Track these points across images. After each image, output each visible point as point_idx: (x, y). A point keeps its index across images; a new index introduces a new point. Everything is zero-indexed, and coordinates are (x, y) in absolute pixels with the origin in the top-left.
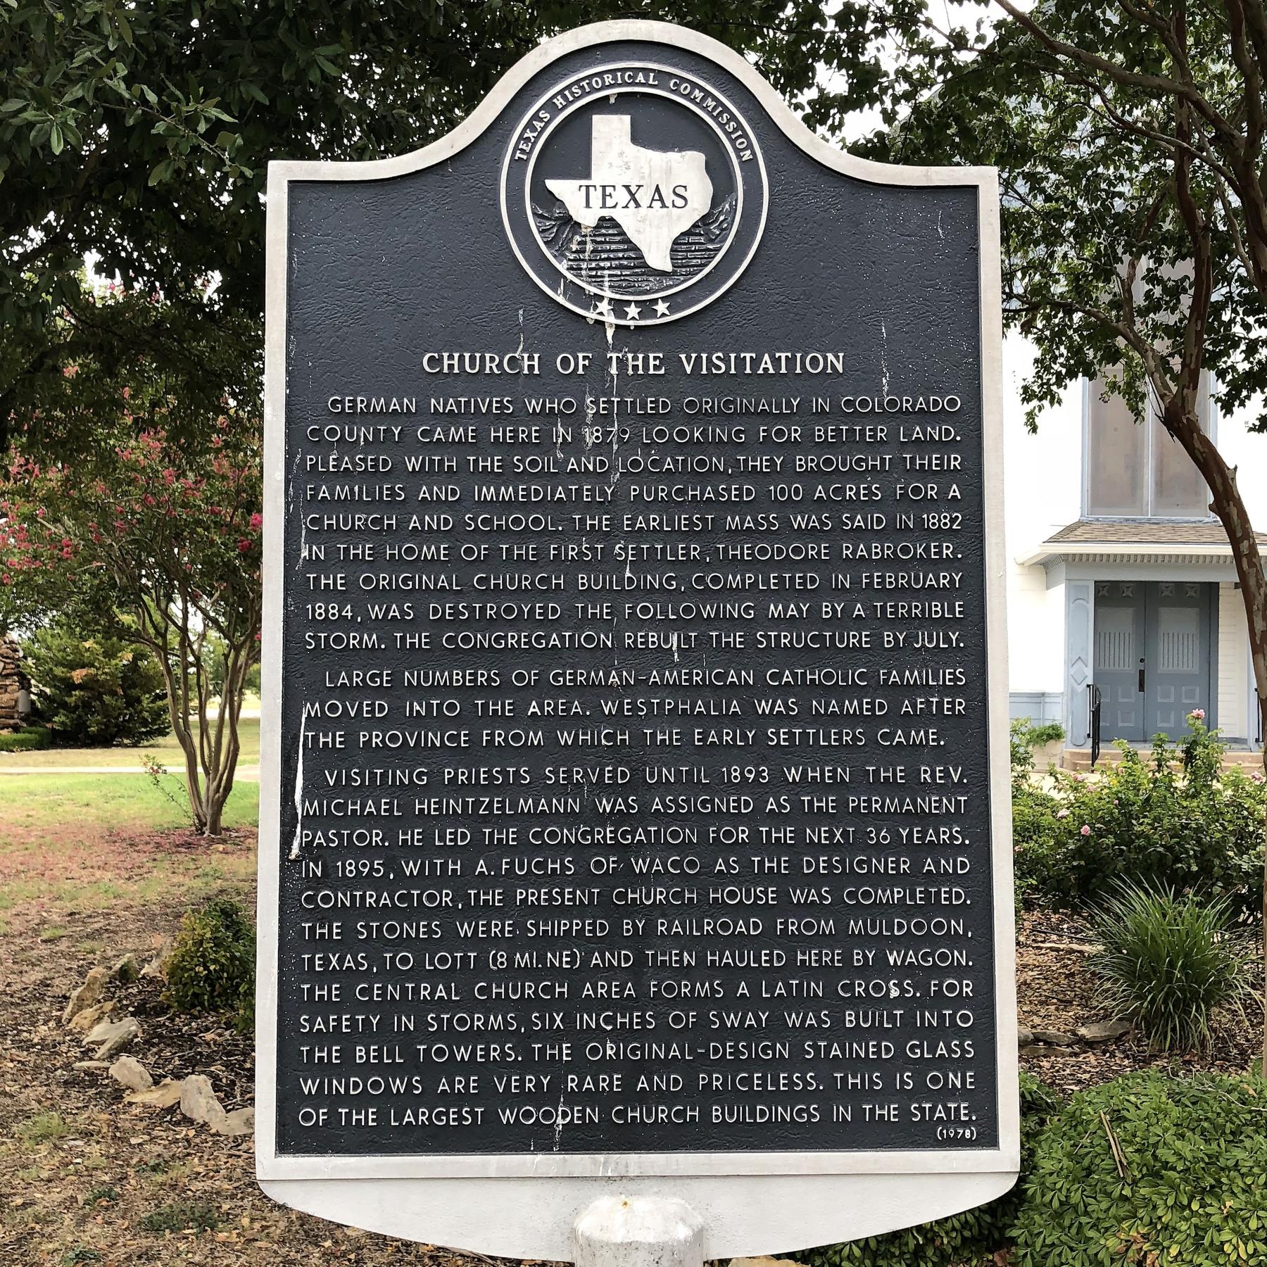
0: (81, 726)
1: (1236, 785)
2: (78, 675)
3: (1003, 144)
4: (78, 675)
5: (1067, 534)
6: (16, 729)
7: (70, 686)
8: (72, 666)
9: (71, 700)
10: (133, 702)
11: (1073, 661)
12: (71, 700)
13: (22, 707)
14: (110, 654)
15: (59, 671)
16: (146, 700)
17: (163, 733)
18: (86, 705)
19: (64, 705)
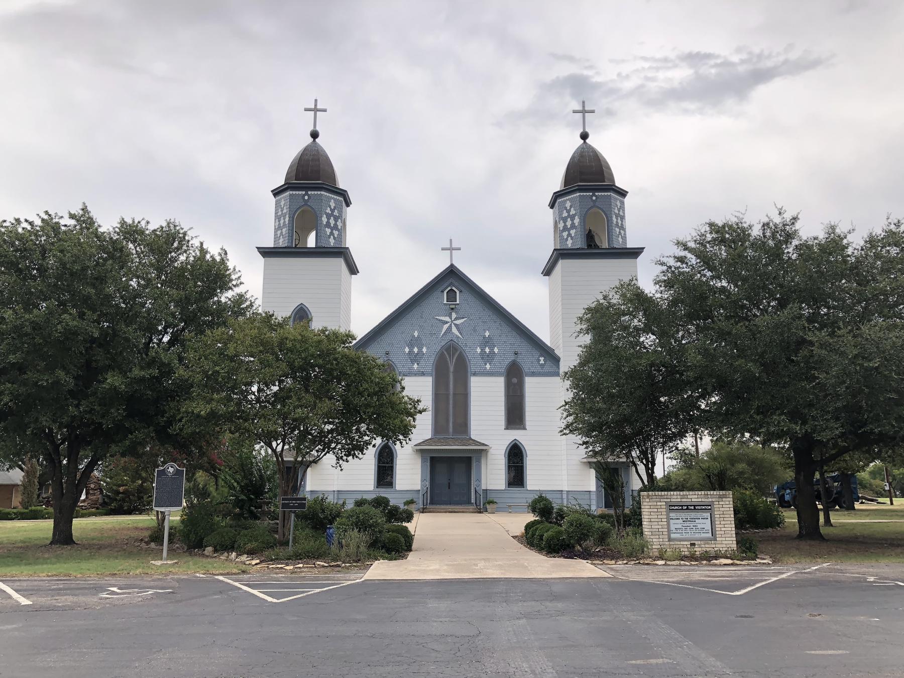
0: (121, 507)
1: (72, 216)
2: (121, 489)
3: (139, 352)
4: (121, 489)
5: (425, 442)
6: (97, 508)
7: (118, 493)
8: (120, 486)
9: (118, 498)
10: (140, 498)
11: (422, 481)
12: (118, 498)
13: (100, 501)
14: (133, 482)
15: (114, 488)
16: (145, 497)
17: (607, 506)
18: (123, 500)
19: (116, 500)
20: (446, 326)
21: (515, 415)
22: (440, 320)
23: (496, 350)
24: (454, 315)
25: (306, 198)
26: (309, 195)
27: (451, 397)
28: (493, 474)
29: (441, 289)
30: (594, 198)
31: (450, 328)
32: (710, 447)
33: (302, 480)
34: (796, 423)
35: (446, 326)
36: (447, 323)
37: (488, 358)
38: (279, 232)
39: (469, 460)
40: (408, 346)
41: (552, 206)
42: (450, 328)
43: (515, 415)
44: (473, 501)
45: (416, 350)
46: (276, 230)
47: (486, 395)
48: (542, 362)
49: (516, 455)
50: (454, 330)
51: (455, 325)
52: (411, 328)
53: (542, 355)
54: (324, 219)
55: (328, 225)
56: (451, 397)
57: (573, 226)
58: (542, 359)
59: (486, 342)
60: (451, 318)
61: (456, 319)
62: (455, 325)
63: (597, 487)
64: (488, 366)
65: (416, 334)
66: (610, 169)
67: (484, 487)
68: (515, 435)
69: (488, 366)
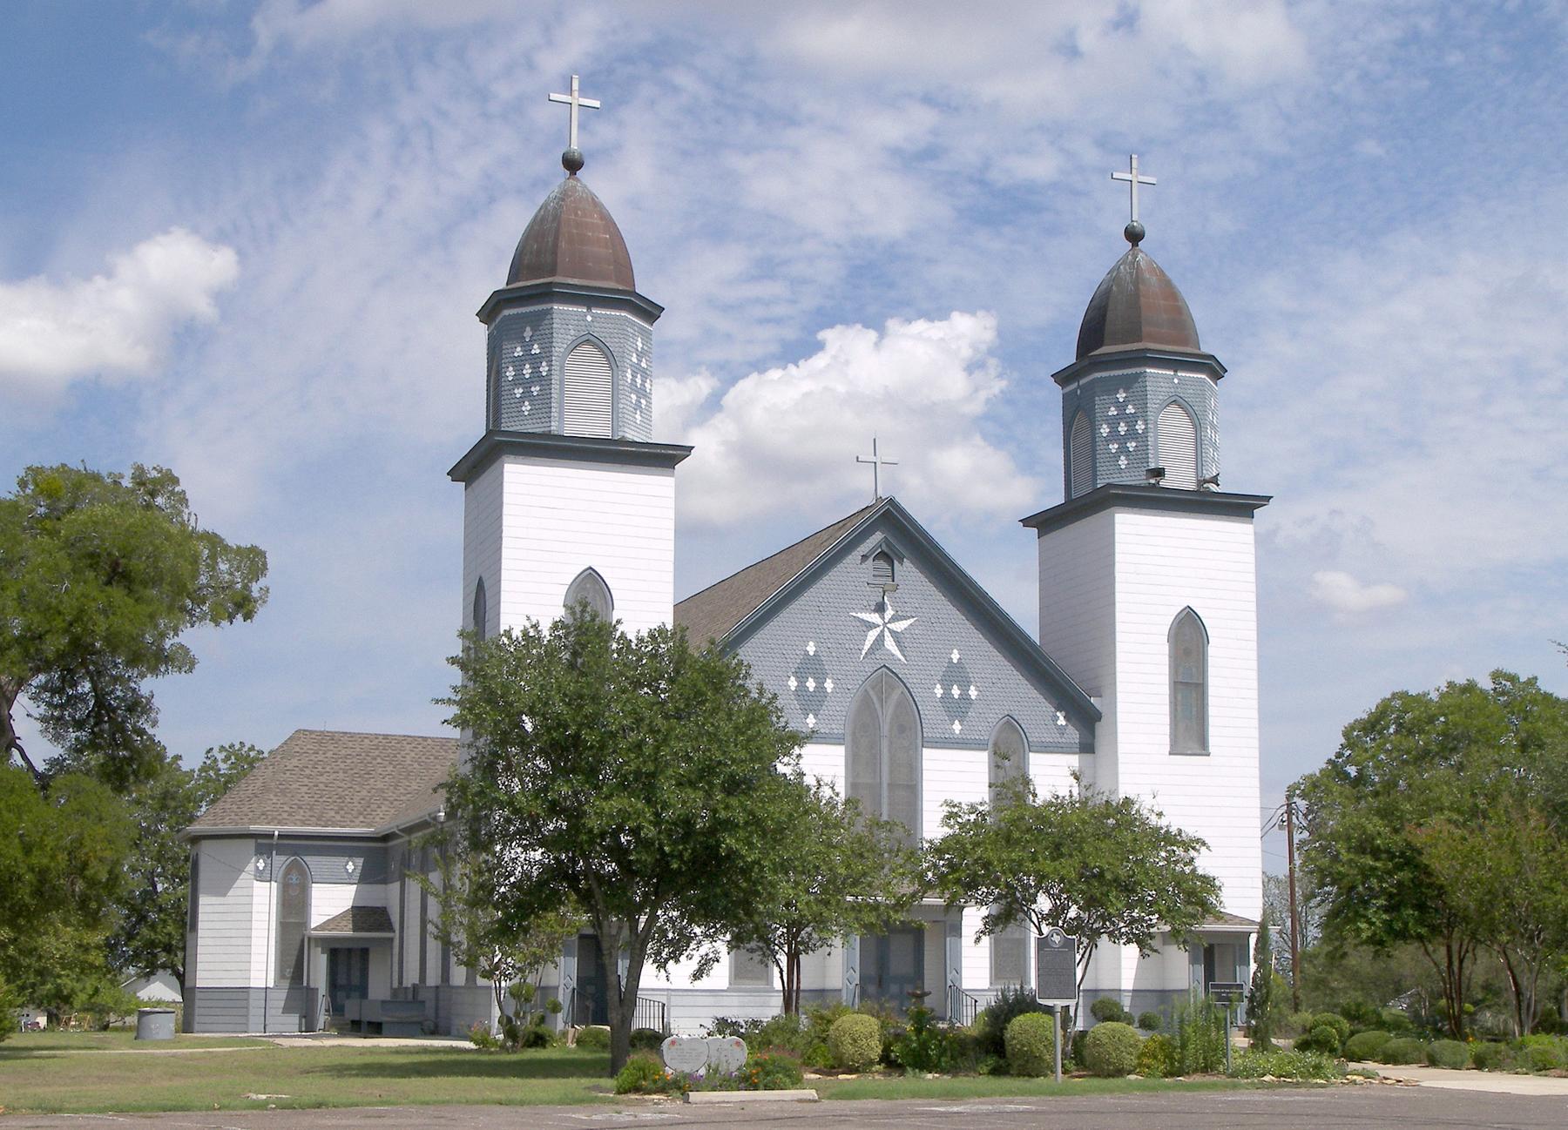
20: (872, 635)
22: (906, 618)
23: (973, 693)
24: (889, 613)
27: (885, 792)
30: (589, 318)
33: (411, 1053)
34: (729, 848)
35: (890, 643)
37: (957, 709)
41: (488, 313)
45: (811, 684)
50: (890, 643)
53: (1058, 709)
55: (1114, 435)
56: (885, 792)
59: (955, 674)
61: (894, 619)
64: (957, 727)
65: (811, 649)
69: (957, 727)
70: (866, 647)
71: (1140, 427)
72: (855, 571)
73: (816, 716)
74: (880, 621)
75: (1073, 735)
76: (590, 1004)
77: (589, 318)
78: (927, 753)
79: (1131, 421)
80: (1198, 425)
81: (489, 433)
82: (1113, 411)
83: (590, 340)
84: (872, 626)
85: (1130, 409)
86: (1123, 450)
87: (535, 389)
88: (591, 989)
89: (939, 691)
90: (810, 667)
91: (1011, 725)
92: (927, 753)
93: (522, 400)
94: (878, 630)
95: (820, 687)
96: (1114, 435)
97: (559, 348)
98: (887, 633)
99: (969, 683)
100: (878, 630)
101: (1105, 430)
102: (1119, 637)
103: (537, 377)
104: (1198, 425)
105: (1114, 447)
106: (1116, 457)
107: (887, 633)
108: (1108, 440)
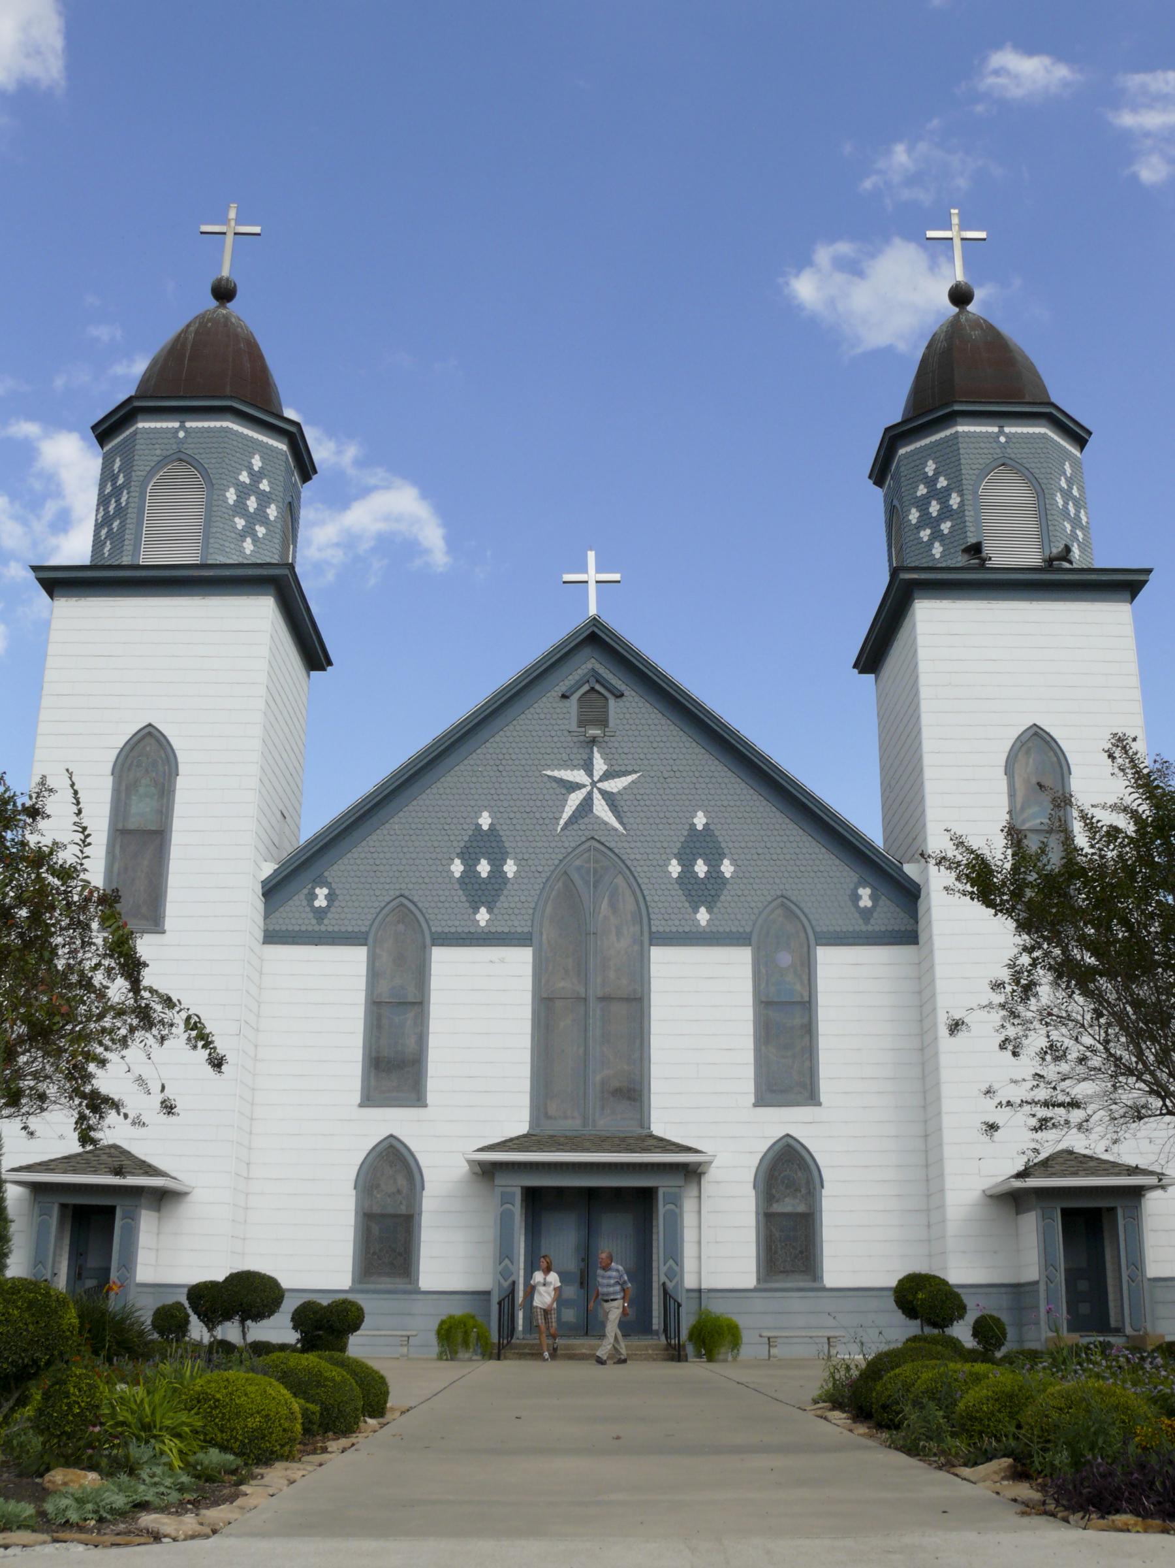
20: (575, 799)
21: (786, 1056)
23: (727, 868)
25: (181, 434)
26: (186, 430)
28: (718, 1247)
29: (562, 688)
30: (181, 434)
31: (588, 802)
32: (876, 338)
35: (601, 809)
36: (579, 786)
38: (104, 532)
39: (647, 1196)
40: (461, 855)
41: (880, 472)
42: (588, 802)
43: (786, 1056)
44: (657, 1322)
45: (484, 868)
46: (98, 527)
47: (699, 1002)
48: (866, 902)
49: (788, 1176)
50: (601, 809)
51: (605, 794)
52: (474, 800)
53: (863, 883)
54: (231, 496)
57: (922, 504)
58: (865, 893)
59: (701, 844)
60: (589, 772)
62: (605, 794)
63: (1047, 1263)
66: (1027, 358)
67: (690, 1282)
68: (393, 1121)
70: (566, 816)
71: (955, 500)
72: (554, 713)
73: (490, 910)
74: (586, 780)
75: (888, 915)
76: (1085, 1309)
77: (1002, 439)
78: (662, 959)
79: (943, 496)
80: (1041, 493)
81: (894, 572)
82: (922, 490)
83: (1006, 463)
84: (574, 787)
85: (942, 482)
86: (937, 535)
87: (946, 527)
88: (1083, 1285)
89: (675, 868)
90: (487, 844)
91: (788, 907)
92: (662, 959)
93: (242, 536)
94: (584, 791)
95: (497, 871)
96: (925, 520)
97: (139, 473)
98: (597, 795)
99: (721, 856)
100: (584, 791)
101: (914, 516)
102: (929, 773)
103: (946, 512)
104: (1041, 493)
105: (925, 534)
106: (930, 544)
107: (597, 795)
108: (919, 527)
